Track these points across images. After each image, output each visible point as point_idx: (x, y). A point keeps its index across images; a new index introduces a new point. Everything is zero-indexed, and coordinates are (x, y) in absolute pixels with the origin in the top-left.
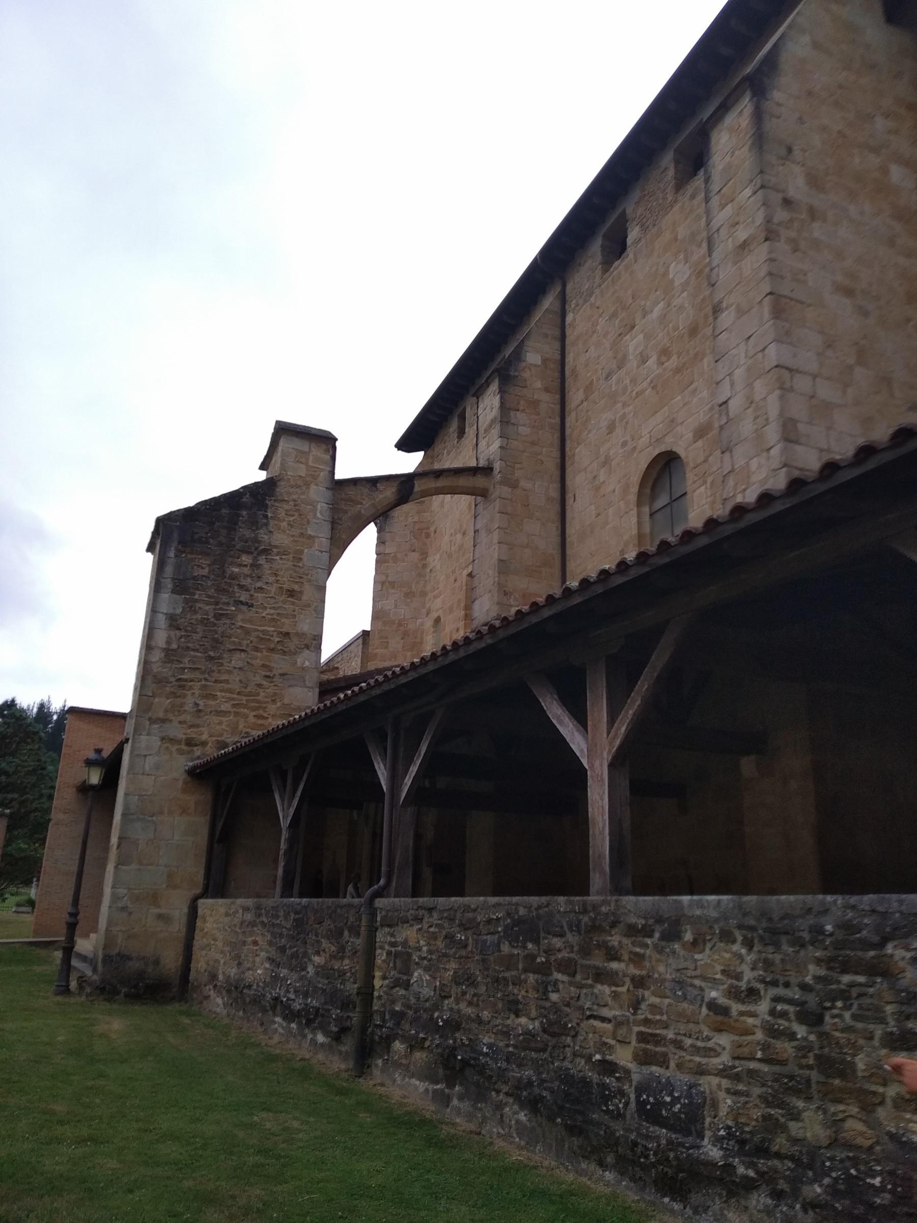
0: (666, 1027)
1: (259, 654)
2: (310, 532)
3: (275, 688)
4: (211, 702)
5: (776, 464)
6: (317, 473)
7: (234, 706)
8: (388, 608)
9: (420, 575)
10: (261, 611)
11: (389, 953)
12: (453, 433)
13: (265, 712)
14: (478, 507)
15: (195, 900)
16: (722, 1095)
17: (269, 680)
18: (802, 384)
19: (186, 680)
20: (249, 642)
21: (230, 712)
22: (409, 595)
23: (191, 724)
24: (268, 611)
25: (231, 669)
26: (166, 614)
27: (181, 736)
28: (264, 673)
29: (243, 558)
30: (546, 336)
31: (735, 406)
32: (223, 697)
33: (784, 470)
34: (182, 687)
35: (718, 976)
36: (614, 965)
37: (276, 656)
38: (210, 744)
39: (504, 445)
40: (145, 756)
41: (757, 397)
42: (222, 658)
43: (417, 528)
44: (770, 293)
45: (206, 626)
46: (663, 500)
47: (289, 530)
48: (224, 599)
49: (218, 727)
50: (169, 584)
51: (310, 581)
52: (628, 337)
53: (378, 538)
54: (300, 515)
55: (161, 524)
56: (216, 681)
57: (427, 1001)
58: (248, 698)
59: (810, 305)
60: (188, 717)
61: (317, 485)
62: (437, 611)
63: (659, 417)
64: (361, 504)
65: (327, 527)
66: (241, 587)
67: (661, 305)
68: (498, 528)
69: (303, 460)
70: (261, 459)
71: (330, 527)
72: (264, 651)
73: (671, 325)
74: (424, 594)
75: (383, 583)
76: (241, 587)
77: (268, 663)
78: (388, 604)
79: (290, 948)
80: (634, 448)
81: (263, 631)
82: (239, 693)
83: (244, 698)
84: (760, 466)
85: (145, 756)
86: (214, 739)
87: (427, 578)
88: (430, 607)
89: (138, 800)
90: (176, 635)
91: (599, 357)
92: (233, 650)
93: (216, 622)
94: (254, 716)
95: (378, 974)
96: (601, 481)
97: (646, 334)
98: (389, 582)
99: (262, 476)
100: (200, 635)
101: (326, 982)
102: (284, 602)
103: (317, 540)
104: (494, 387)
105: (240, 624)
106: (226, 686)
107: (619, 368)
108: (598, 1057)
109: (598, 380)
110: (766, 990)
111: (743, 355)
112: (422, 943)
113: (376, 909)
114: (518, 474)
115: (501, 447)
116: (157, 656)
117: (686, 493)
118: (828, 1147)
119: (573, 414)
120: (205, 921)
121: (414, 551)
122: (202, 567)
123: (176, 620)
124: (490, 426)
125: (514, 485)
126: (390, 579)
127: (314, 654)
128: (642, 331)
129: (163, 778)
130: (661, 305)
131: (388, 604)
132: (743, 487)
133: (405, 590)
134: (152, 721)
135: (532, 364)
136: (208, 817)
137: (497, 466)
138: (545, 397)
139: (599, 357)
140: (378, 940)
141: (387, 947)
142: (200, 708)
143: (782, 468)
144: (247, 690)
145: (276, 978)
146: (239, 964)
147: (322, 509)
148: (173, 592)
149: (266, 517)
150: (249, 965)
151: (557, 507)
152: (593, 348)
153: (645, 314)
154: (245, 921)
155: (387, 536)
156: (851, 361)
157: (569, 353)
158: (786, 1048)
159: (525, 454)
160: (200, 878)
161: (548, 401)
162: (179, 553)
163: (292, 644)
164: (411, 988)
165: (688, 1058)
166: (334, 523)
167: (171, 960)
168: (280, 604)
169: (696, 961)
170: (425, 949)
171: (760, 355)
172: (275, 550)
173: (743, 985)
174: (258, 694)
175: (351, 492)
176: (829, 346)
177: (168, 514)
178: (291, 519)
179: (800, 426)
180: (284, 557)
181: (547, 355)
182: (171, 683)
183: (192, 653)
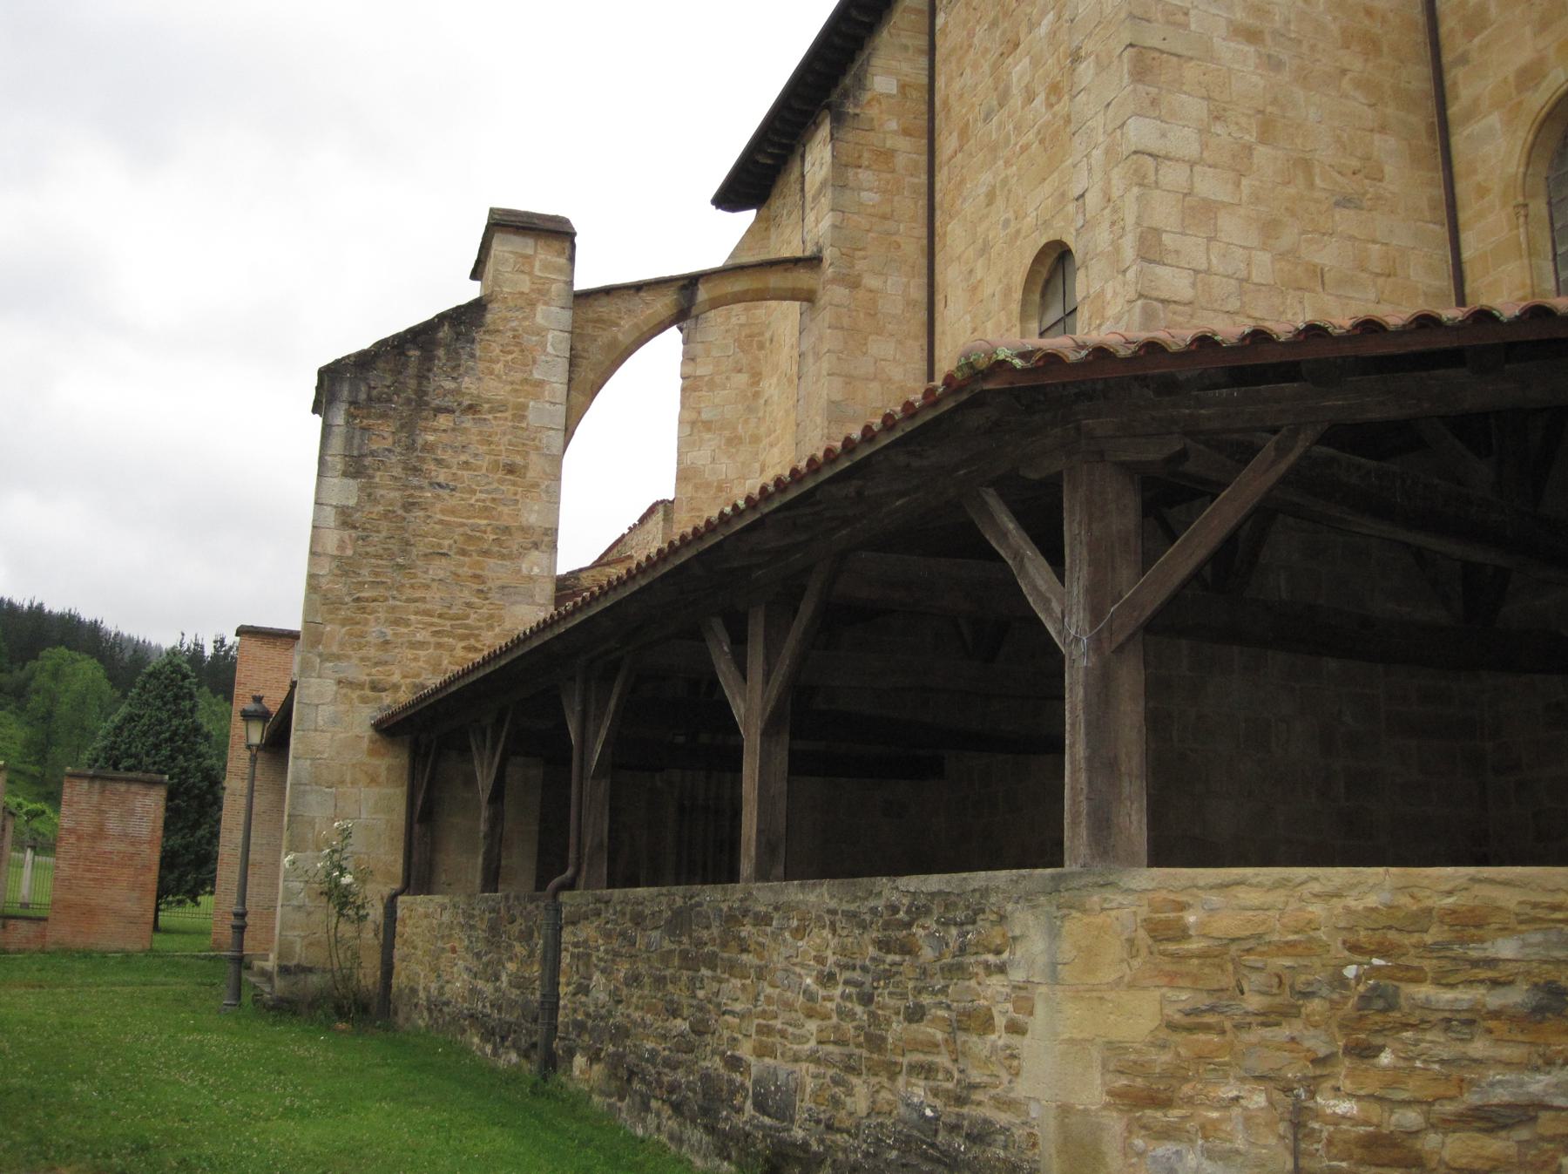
0: (776, 1017)
1: (467, 559)
2: (537, 376)
3: (492, 607)
4: (403, 630)
5: (1132, 295)
6: (546, 286)
7: (435, 633)
8: (700, 463)
9: (750, 410)
10: (468, 496)
11: (572, 956)
12: (795, 182)
13: (478, 641)
14: (804, 316)
15: (393, 899)
16: (808, 1080)
17: (481, 596)
18: (1173, 176)
19: (367, 600)
20: (451, 542)
21: (429, 643)
22: (734, 441)
23: (376, 660)
24: (479, 495)
25: (428, 582)
26: (336, 507)
27: (364, 678)
28: (476, 587)
29: (441, 420)
30: (905, 48)
31: (1093, 199)
32: (419, 623)
33: (1139, 302)
34: (363, 610)
35: (812, 963)
36: (744, 957)
37: (491, 561)
38: (403, 688)
39: (837, 223)
40: (317, 706)
41: (1115, 194)
42: (415, 568)
43: (743, 334)
44: (1131, 45)
45: (391, 522)
46: (1055, 314)
47: (506, 374)
48: (415, 481)
49: (413, 664)
50: (337, 463)
51: (537, 449)
52: (1010, 60)
53: (685, 353)
54: (522, 351)
55: (326, 379)
56: (408, 600)
57: (603, 1007)
58: (454, 622)
59: (1191, 59)
60: (372, 652)
61: (546, 303)
62: (774, 466)
63: (1047, 188)
64: (617, 325)
65: (563, 365)
66: (439, 462)
67: (1051, 16)
68: (829, 351)
69: (527, 269)
70: (472, 266)
71: (567, 366)
72: (474, 554)
73: (1061, 49)
74: (755, 439)
75: (693, 423)
76: (439, 462)
77: (478, 572)
78: (701, 457)
79: (486, 954)
80: (1018, 232)
81: (472, 525)
82: (440, 616)
83: (448, 623)
84: (1115, 294)
85: (317, 706)
86: (408, 681)
87: (761, 414)
88: (764, 461)
89: (311, 765)
90: (350, 536)
91: (976, 85)
92: (431, 554)
93: (405, 514)
94: (464, 648)
95: (562, 980)
96: (979, 278)
97: (1032, 57)
98: (703, 422)
99: (473, 291)
100: (384, 534)
101: (518, 992)
102: (501, 481)
103: (547, 387)
104: (824, 131)
105: (439, 516)
106: (421, 606)
107: (1001, 106)
108: (729, 1053)
109: (976, 121)
110: (841, 974)
111: (1101, 130)
112: (600, 941)
113: (561, 905)
114: (860, 265)
115: (834, 226)
116: (325, 568)
117: (1076, 309)
118: (869, 1115)
119: (945, 169)
120: (405, 925)
121: (740, 371)
122: (384, 436)
123: (350, 516)
124: (819, 192)
125: (854, 284)
126: (704, 416)
127: (545, 556)
128: (1029, 52)
129: (342, 735)
130: (1051, 16)
131: (701, 457)
132: (1098, 322)
133: (727, 433)
134: (325, 658)
135: (881, 94)
136: (405, 788)
137: (827, 254)
138: (903, 144)
139: (976, 85)
140: (563, 940)
141: (571, 948)
142: (388, 638)
143: (1137, 300)
144: (451, 612)
145: (473, 991)
146: (439, 976)
147: (556, 343)
148: (345, 474)
149: (472, 356)
150: (448, 978)
151: (923, 316)
152: (968, 71)
153: (1032, 26)
154: (443, 923)
155: (698, 349)
156: (1250, 138)
157: (939, 75)
158: (849, 1027)
159: (871, 235)
160: (398, 868)
161: (908, 151)
162: (351, 416)
163: (515, 543)
164: (590, 995)
165: (789, 1046)
166: (573, 361)
167: (368, 975)
168: (495, 485)
169: (798, 948)
170: (602, 948)
171: (1118, 132)
172: (486, 406)
173: (827, 970)
174: (467, 617)
175: (604, 308)
176: (1217, 118)
177: (333, 363)
178: (510, 357)
179: (1164, 236)
180: (499, 415)
181: (907, 79)
182: (347, 604)
183: (373, 561)
